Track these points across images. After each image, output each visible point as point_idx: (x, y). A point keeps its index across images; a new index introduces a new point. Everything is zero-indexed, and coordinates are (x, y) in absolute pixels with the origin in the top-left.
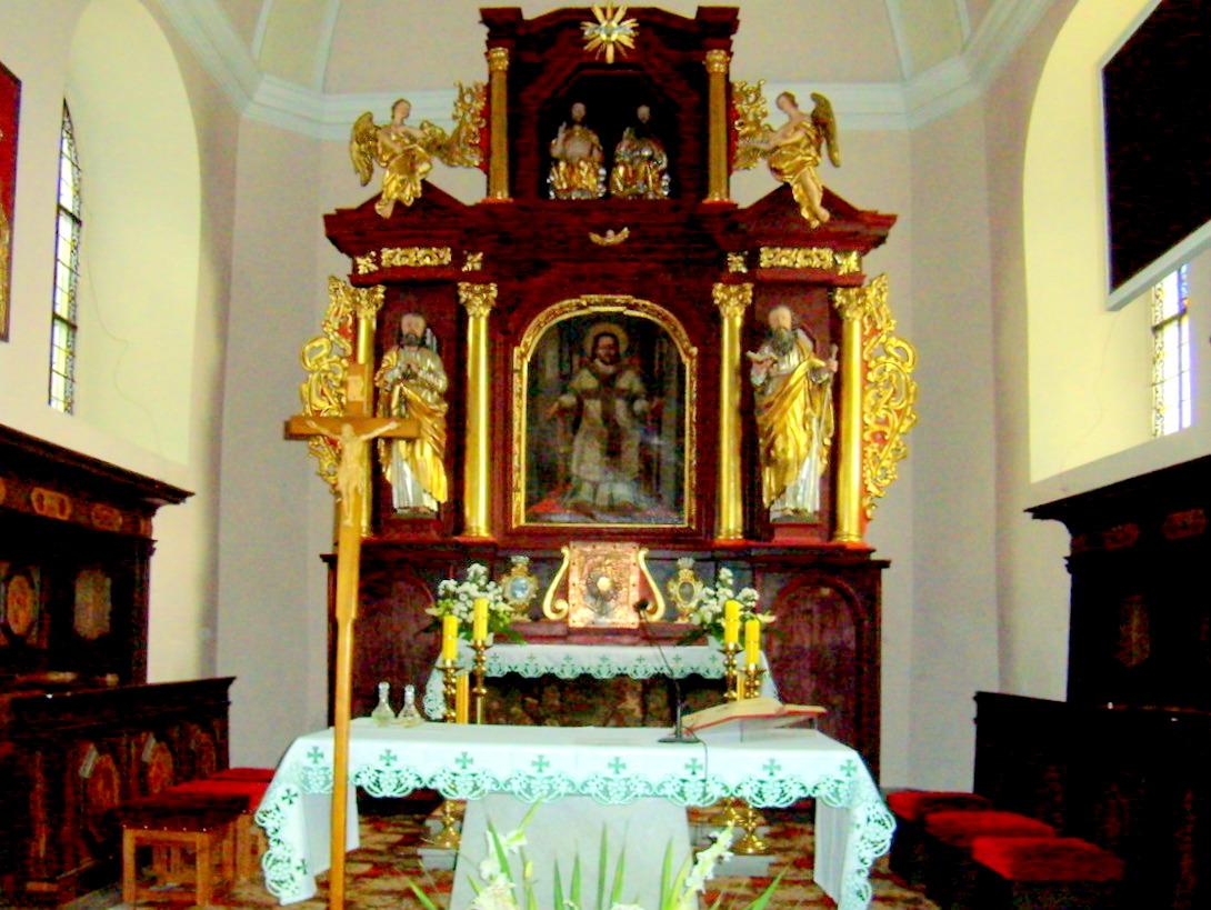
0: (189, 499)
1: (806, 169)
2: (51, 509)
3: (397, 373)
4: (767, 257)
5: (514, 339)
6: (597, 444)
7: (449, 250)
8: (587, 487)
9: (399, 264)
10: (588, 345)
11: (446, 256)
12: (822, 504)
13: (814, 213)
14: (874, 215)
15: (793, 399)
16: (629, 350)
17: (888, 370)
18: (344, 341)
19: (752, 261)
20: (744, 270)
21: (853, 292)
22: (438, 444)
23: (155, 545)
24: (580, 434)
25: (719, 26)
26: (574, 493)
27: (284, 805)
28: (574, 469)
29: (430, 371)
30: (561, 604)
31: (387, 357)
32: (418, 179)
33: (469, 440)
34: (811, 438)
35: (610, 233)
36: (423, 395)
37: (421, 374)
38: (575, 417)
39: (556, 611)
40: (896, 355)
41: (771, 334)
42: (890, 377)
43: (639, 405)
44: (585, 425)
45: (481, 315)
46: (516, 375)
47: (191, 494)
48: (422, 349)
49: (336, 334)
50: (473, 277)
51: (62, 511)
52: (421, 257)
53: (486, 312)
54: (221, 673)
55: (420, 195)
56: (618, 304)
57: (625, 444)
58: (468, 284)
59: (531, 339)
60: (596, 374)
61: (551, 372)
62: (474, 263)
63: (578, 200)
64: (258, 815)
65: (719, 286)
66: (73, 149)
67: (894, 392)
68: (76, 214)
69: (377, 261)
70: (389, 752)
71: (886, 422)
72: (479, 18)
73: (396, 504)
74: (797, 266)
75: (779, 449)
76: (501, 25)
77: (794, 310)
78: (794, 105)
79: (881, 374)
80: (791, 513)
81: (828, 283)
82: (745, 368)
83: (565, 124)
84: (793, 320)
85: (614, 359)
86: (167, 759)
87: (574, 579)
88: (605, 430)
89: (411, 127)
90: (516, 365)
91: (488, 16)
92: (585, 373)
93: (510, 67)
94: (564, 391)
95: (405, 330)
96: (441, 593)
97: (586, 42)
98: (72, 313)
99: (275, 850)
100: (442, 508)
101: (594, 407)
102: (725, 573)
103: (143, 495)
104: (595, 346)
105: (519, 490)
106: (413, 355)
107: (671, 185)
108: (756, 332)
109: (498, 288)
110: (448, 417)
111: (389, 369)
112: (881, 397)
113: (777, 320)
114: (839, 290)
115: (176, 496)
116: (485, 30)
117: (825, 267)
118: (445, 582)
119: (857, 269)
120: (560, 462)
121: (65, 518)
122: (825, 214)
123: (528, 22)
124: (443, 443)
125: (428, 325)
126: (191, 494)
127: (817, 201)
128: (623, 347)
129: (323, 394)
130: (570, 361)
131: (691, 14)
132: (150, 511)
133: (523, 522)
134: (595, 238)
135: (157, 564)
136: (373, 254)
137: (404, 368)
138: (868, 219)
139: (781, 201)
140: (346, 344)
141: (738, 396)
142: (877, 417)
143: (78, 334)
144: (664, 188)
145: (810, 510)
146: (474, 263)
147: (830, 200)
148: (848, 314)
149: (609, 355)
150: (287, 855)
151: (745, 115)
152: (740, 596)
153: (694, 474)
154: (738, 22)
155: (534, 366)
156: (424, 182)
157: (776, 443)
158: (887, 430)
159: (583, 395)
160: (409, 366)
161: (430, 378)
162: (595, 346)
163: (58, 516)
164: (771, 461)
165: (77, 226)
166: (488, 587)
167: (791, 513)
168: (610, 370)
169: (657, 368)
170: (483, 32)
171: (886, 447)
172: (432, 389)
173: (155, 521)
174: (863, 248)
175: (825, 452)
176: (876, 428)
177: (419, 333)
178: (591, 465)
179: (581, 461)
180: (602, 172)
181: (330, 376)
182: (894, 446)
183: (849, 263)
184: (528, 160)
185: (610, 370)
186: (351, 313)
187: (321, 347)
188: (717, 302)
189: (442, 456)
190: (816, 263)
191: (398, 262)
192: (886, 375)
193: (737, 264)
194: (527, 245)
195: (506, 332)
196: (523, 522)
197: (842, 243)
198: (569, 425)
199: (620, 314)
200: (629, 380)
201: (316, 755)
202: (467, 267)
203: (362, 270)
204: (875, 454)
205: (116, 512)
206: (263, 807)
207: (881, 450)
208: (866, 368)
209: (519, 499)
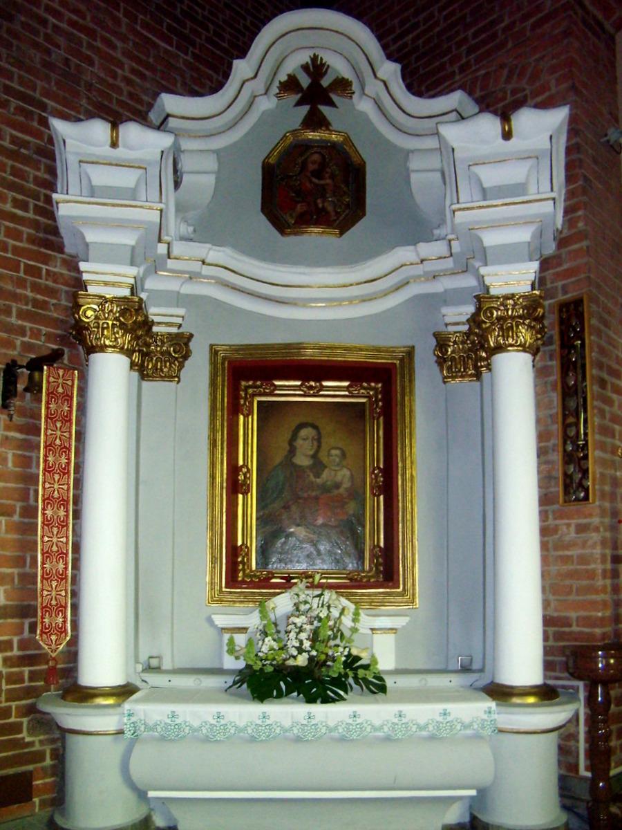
91: (413, 347)
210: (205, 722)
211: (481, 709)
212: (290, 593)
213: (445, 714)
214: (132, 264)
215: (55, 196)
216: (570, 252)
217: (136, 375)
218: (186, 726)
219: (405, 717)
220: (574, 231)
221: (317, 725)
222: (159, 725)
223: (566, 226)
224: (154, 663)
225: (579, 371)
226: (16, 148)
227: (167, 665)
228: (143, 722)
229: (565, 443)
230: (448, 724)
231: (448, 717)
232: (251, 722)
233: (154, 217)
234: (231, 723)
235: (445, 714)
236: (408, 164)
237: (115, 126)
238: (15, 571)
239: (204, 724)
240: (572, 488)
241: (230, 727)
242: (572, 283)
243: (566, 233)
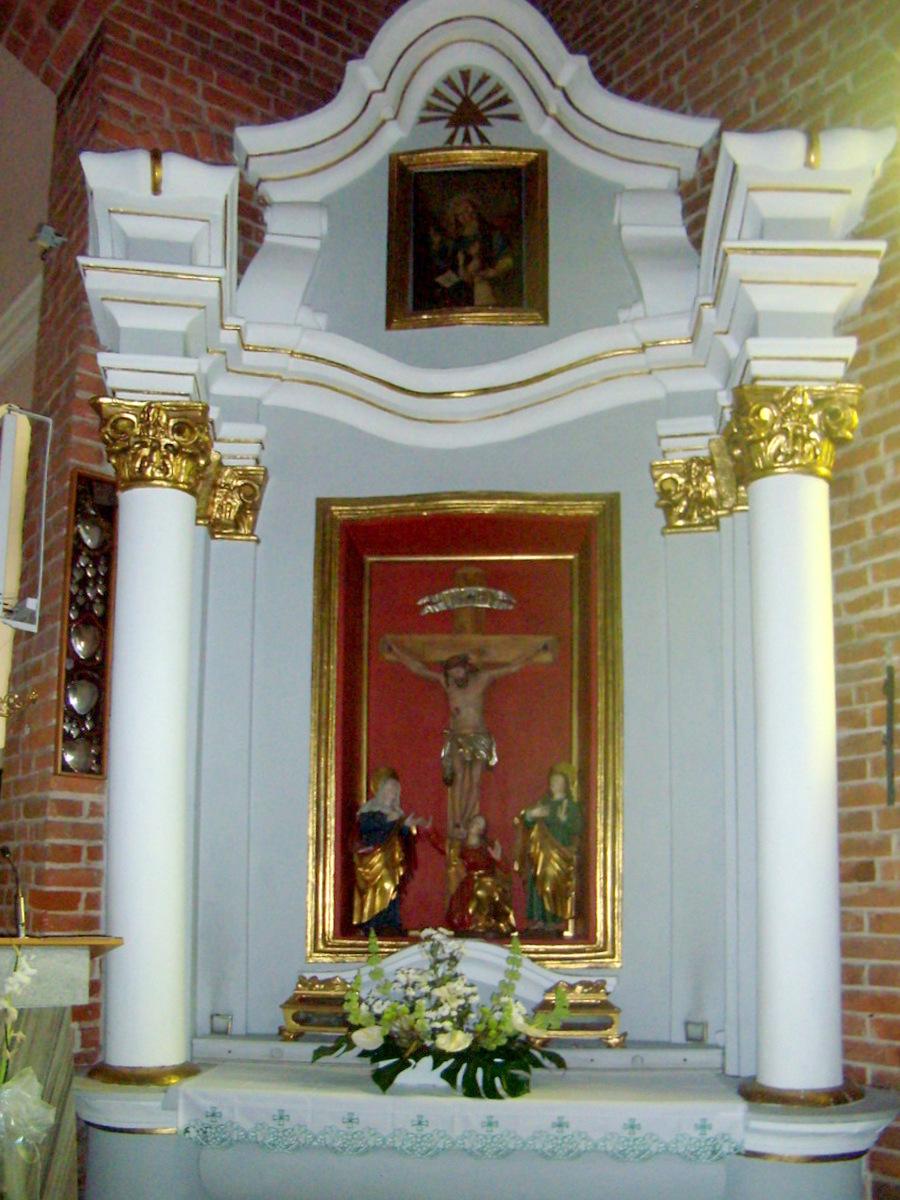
159: (784, 431)
211: (731, 1116)
213: (420, 1123)
214: (186, 354)
215: (82, 260)
217: (203, 530)
218: (726, 1141)
219: (358, 1123)
221: (362, 1133)
224: (220, 1023)
226: (23, 920)
227: (238, 1028)
230: (709, 1143)
231: (494, 1129)
233: (212, 291)
234: (370, 1129)
235: (281, 1118)
236: (42, 1087)
237: (156, 157)
238: (50, 818)
240: (556, 861)
241: (507, 1139)
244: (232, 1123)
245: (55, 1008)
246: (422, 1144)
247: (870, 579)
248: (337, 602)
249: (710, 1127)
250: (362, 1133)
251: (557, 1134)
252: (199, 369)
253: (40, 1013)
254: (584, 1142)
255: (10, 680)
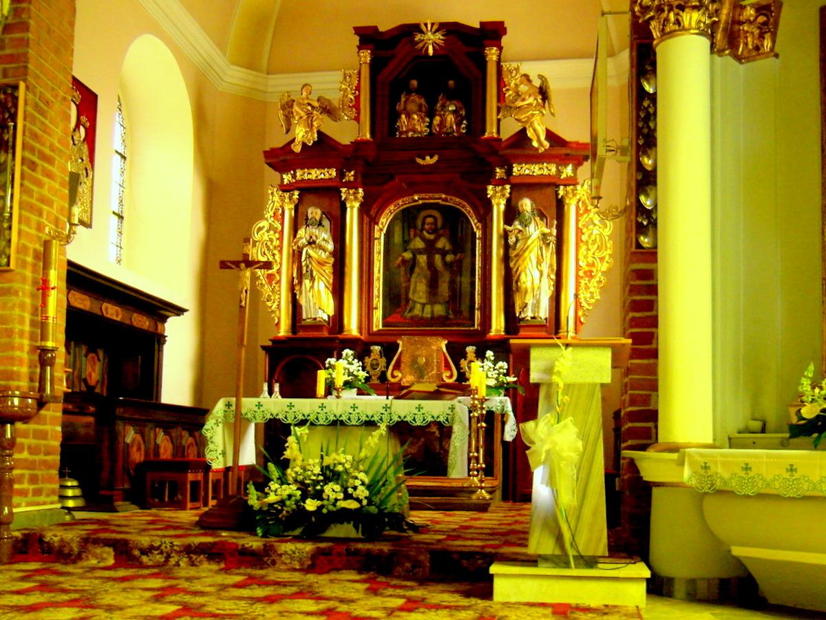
0: (185, 313)
1: (534, 118)
2: (112, 315)
3: (304, 241)
4: (516, 169)
5: (374, 221)
6: (424, 281)
7: (335, 169)
8: (418, 306)
9: (306, 178)
10: (419, 223)
11: (333, 173)
12: (550, 313)
13: (539, 142)
14: (577, 143)
15: (530, 252)
16: (443, 227)
17: (594, 233)
18: (276, 222)
19: (509, 172)
20: (505, 178)
21: (569, 188)
22: (328, 282)
23: (166, 338)
24: (414, 276)
25: (493, 32)
26: (411, 310)
27: (215, 427)
28: (411, 296)
29: (324, 240)
30: (396, 373)
31: (299, 232)
32: (315, 131)
33: (347, 280)
34: (541, 275)
35: (428, 158)
36: (319, 254)
37: (317, 241)
38: (411, 266)
39: (393, 376)
40: (600, 225)
41: (519, 213)
42: (596, 238)
43: (449, 258)
44: (417, 270)
45: (354, 207)
46: (376, 242)
47: (186, 310)
48: (320, 227)
49: (272, 219)
50: (349, 185)
51: (117, 316)
52: (315, 174)
53: (357, 205)
54: (204, 407)
55: (316, 139)
56: (440, 198)
57: (440, 281)
58: (346, 189)
59: (384, 221)
60: (423, 239)
61: (397, 238)
62: (350, 176)
63: (412, 138)
64: (204, 431)
65: (490, 187)
66: (121, 116)
67: (598, 246)
68: (123, 153)
69: (294, 176)
70: (259, 403)
71: (593, 265)
72: (353, 32)
73: (304, 317)
74: (535, 174)
75: (522, 282)
76: (368, 37)
77: (533, 200)
78: (529, 81)
79: (590, 237)
80: (529, 319)
81: (552, 184)
82: (506, 235)
83: (405, 93)
84: (532, 206)
85: (434, 231)
86: (170, 446)
87: (405, 359)
88: (429, 272)
89: (311, 100)
90: (376, 235)
91: (358, 31)
92: (418, 239)
93: (371, 61)
94: (405, 250)
95: (310, 216)
96: (327, 365)
97: (417, 43)
98: (120, 210)
99: (211, 446)
100: (331, 319)
101: (422, 259)
102: (489, 354)
103: (160, 310)
104: (423, 223)
105: (376, 308)
106: (314, 231)
107: (467, 127)
108: (512, 214)
109: (364, 191)
110: (334, 266)
111: (301, 238)
112: (589, 250)
113: (522, 206)
114: (562, 187)
115: (179, 311)
116: (357, 38)
117: (551, 174)
118: (329, 360)
119: (572, 175)
120: (403, 291)
121: (118, 319)
122: (547, 144)
123: (382, 32)
124: (331, 281)
125: (323, 213)
126: (186, 310)
127: (543, 137)
128: (439, 224)
129: (265, 254)
130: (409, 234)
131: (477, 26)
132: (164, 319)
133: (381, 327)
134: (419, 161)
135: (167, 348)
136: (292, 172)
137: (308, 238)
138: (574, 146)
139: (521, 138)
140: (278, 225)
141: (502, 252)
142: (588, 262)
143: (124, 221)
144: (463, 129)
145: (543, 317)
146: (350, 176)
147: (550, 135)
148: (567, 201)
149: (431, 228)
150: (216, 448)
151: (510, 84)
152: (497, 367)
153: (479, 296)
154: (506, 29)
155: (389, 236)
156: (319, 133)
157: (521, 278)
158: (594, 269)
159: (416, 252)
160: (311, 237)
161: (323, 243)
162: (423, 223)
163: (115, 318)
164: (518, 289)
165: (123, 160)
166: (353, 362)
167: (529, 319)
168: (432, 237)
169: (460, 234)
170: (356, 40)
171: (593, 280)
172: (325, 250)
173: (166, 325)
174: (576, 162)
175: (552, 283)
176: (587, 269)
177: (318, 218)
178: (421, 294)
179: (414, 292)
180: (428, 120)
181: (269, 243)
182: (597, 279)
183: (568, 171)
184: (384, 111)
185: (432, 237)
186: (280, 206)
187: (264, 227)
188: (489, 196)
189: (331, 289)
190: (546, 172)
191: (306, 177)
192: (593, 237)
193: (499, 172)
194: (377, 166)
195: (369, 216)
196: (381, 327)
197: (563, 160)
198: (408, 269)
199: (438, 204)
200: (442, 243)
201: (229, 405)
202: (346, 179)
203: (286, 182)
204: (586, 284)
205: (145, 318)
206: (206, 427)
207: (589, 282)
208: (579, 232)
209: (378, 315)
210: (735, 474)
212: (142, 325)
216: (12, 40)
220: (18, 20)
222: (777, 480)
223: (12, 13)
225: (10, 151)
228: (806, 479)
229: (638, 138)
232: (778, 476)
234: (805, 477)
239: (733, 476)
241: (803, 482)
242: (14, 68)
243: (10, 21)
244: (717, 474)
245: (590, 384)
246: (793, 486)
247: (31, 491)
248: (314, 333)
249: (796, 470)
250: (754, 477)
251: (744, 476)
252: (125, 426)
253: (581, 386)
254: (807, 484)
255: (655, 139)
